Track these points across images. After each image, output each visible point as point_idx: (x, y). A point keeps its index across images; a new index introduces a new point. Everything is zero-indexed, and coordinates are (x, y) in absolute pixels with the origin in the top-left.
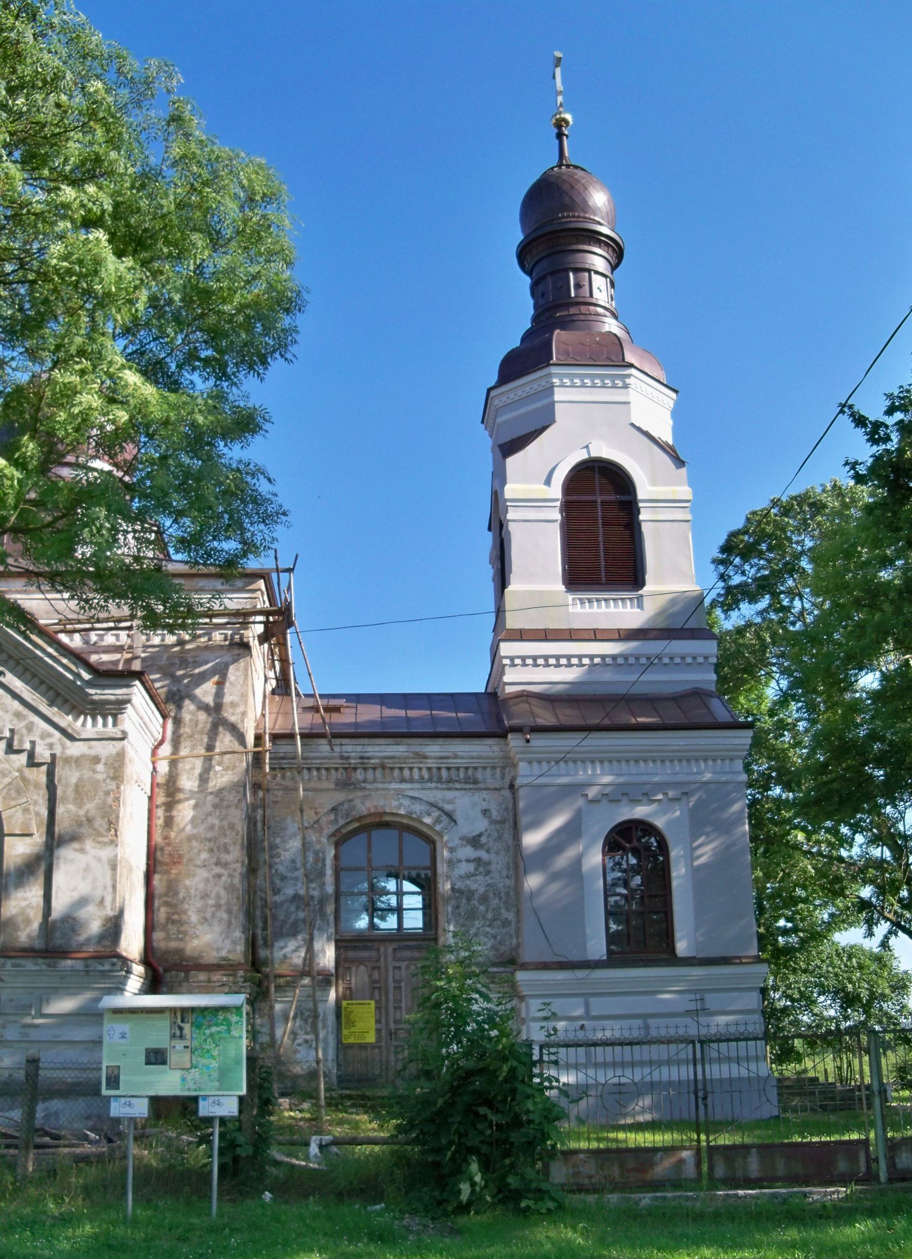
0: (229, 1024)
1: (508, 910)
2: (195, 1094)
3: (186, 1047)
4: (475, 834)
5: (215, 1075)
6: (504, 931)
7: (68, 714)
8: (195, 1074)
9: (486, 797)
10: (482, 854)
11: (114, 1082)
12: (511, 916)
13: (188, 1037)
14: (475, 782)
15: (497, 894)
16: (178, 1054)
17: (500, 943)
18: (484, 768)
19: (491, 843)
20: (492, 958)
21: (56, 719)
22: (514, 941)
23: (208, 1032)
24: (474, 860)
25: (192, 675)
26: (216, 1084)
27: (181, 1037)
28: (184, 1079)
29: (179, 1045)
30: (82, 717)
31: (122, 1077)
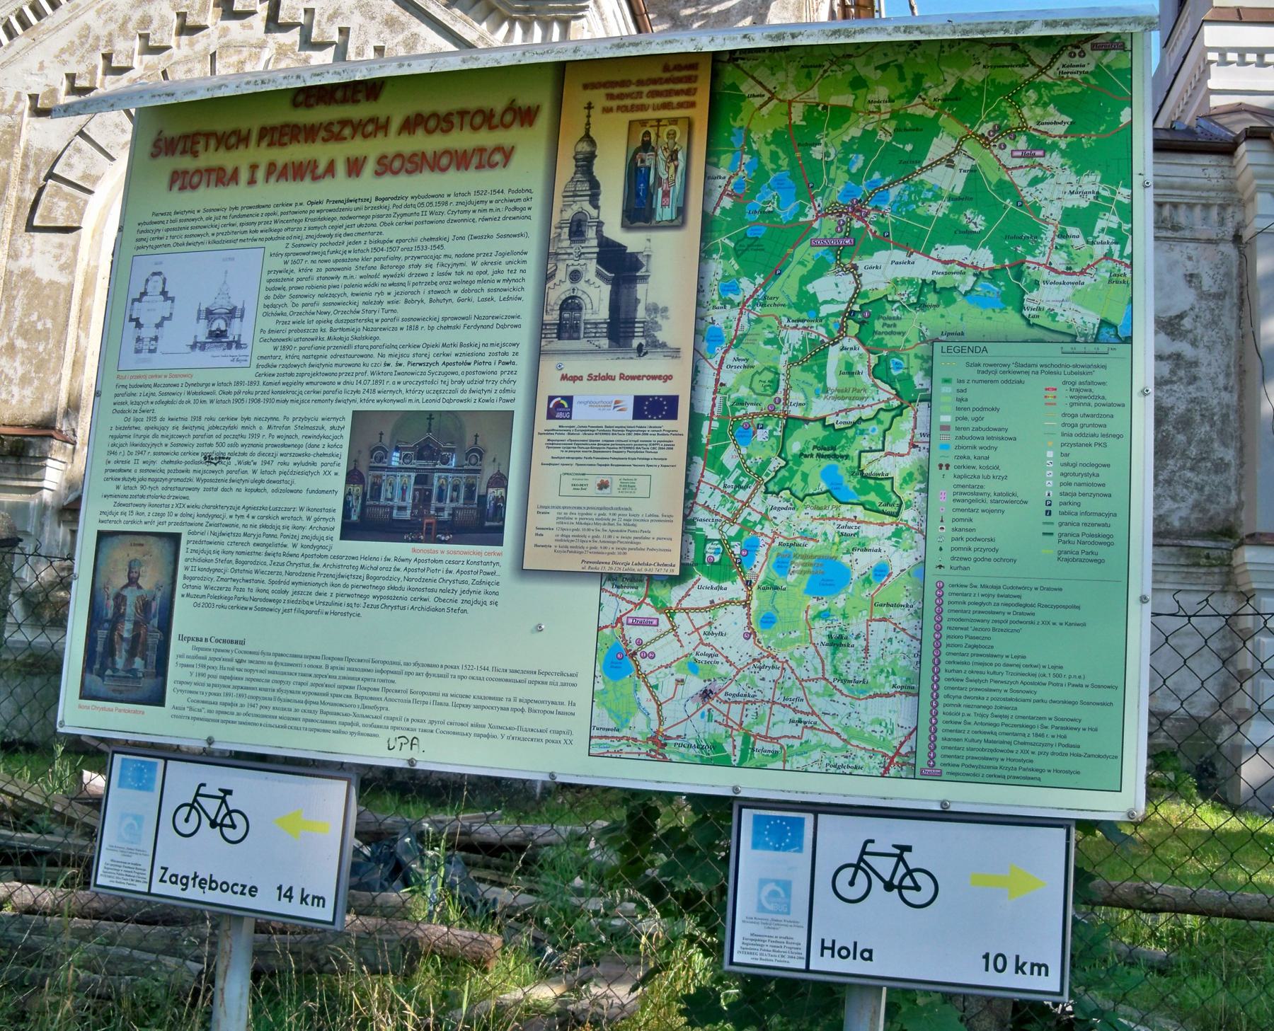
0: (1016, 230)
1: (1225, 445)
2: (714, 781)
3: (648, 408)
4: (1173, 313)
5: (887, 644)
6: (1217, 479)
7: (480, 22)
8: (716, 622)
9: (1193, 253)
10: (1184, 347)
11: (134, 651)
12: (1229, 455)
13: (676, 330)
14: (1175, 228)
15: (1207, 416)
16: (588, 474)
17: (1210, 499)
18: (1190, 206)
19: (1199, 331)
20: (1194, 524)
21: (458, 28)
22: (1233, 498)
23: (833, 290)
24: (1170, 357)
25: (706, 16)
26: (894, 714)
27: (621, 329)
28: (621, 660)
29: (603, 387)
30: (506, 26)
31: (186, 618)
